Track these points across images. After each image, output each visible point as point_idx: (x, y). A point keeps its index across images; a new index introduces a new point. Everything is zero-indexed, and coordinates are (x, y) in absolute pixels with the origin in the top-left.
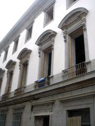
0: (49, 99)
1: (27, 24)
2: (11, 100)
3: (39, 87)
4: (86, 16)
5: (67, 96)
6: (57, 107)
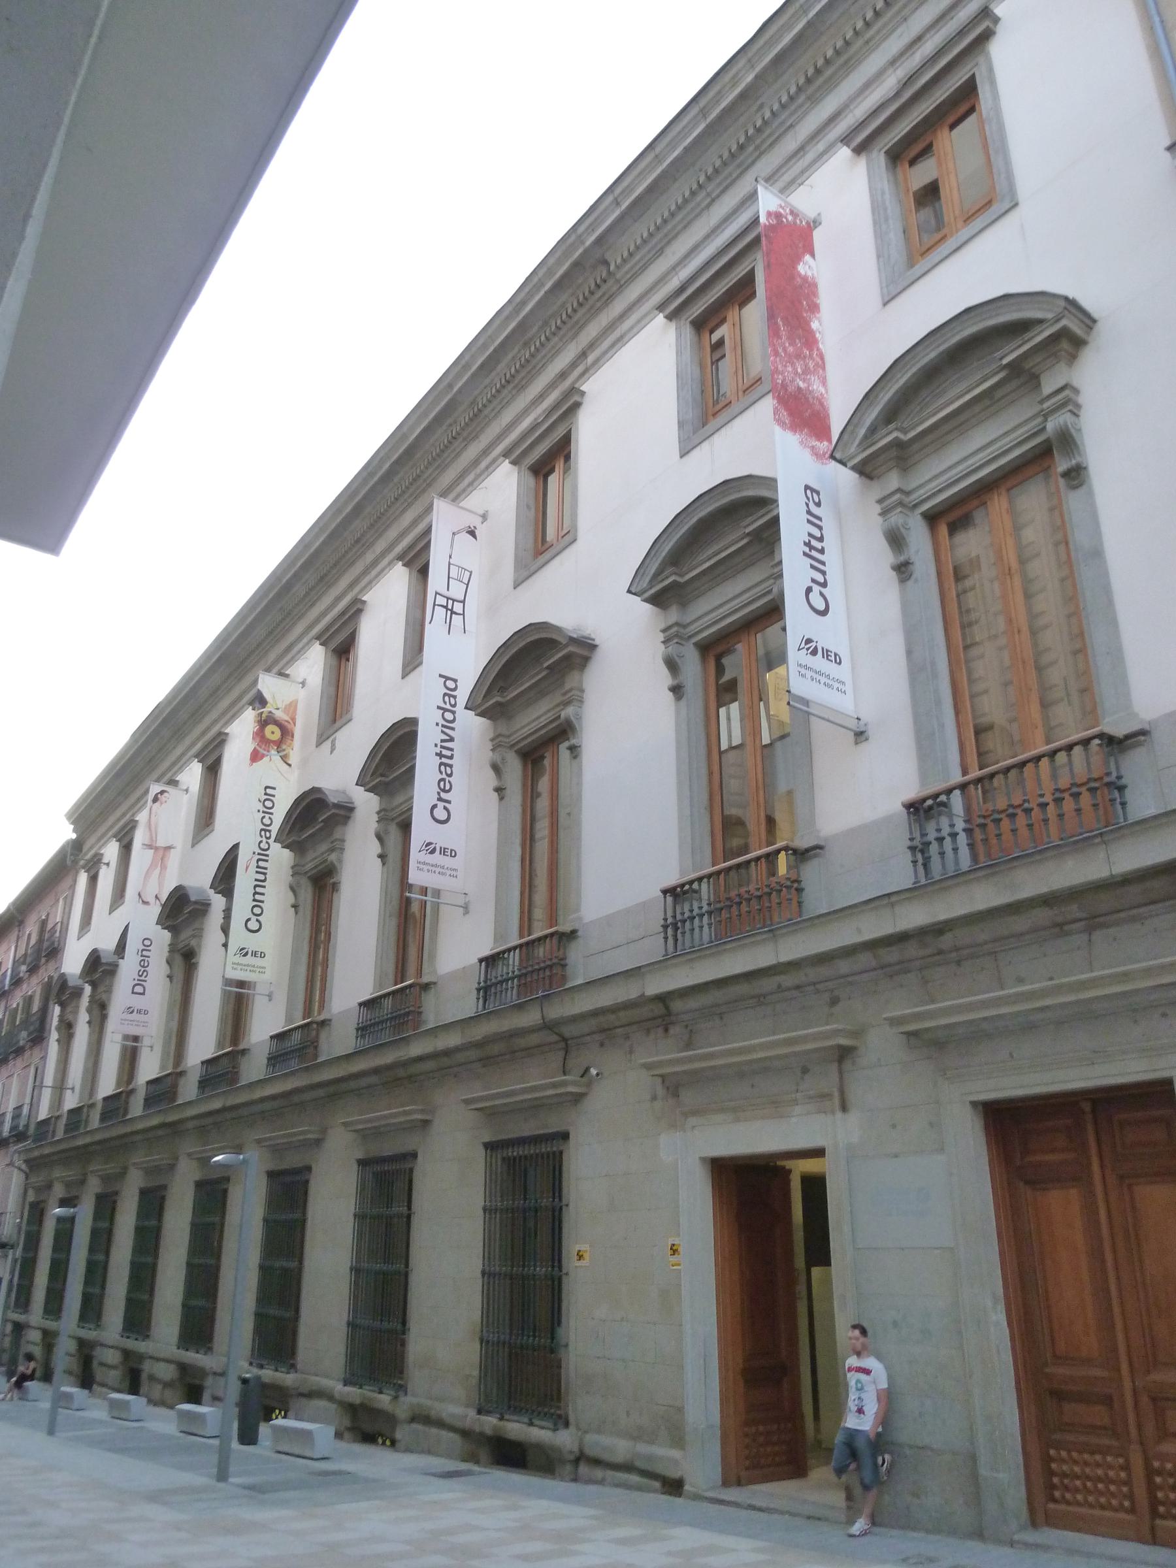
0: (818, 1030)
1: (522, 413)
2: (452, 1040)
3: (524, 987)
4: (1073, 358)
5: (959, 999)
6: (885, 1073)
